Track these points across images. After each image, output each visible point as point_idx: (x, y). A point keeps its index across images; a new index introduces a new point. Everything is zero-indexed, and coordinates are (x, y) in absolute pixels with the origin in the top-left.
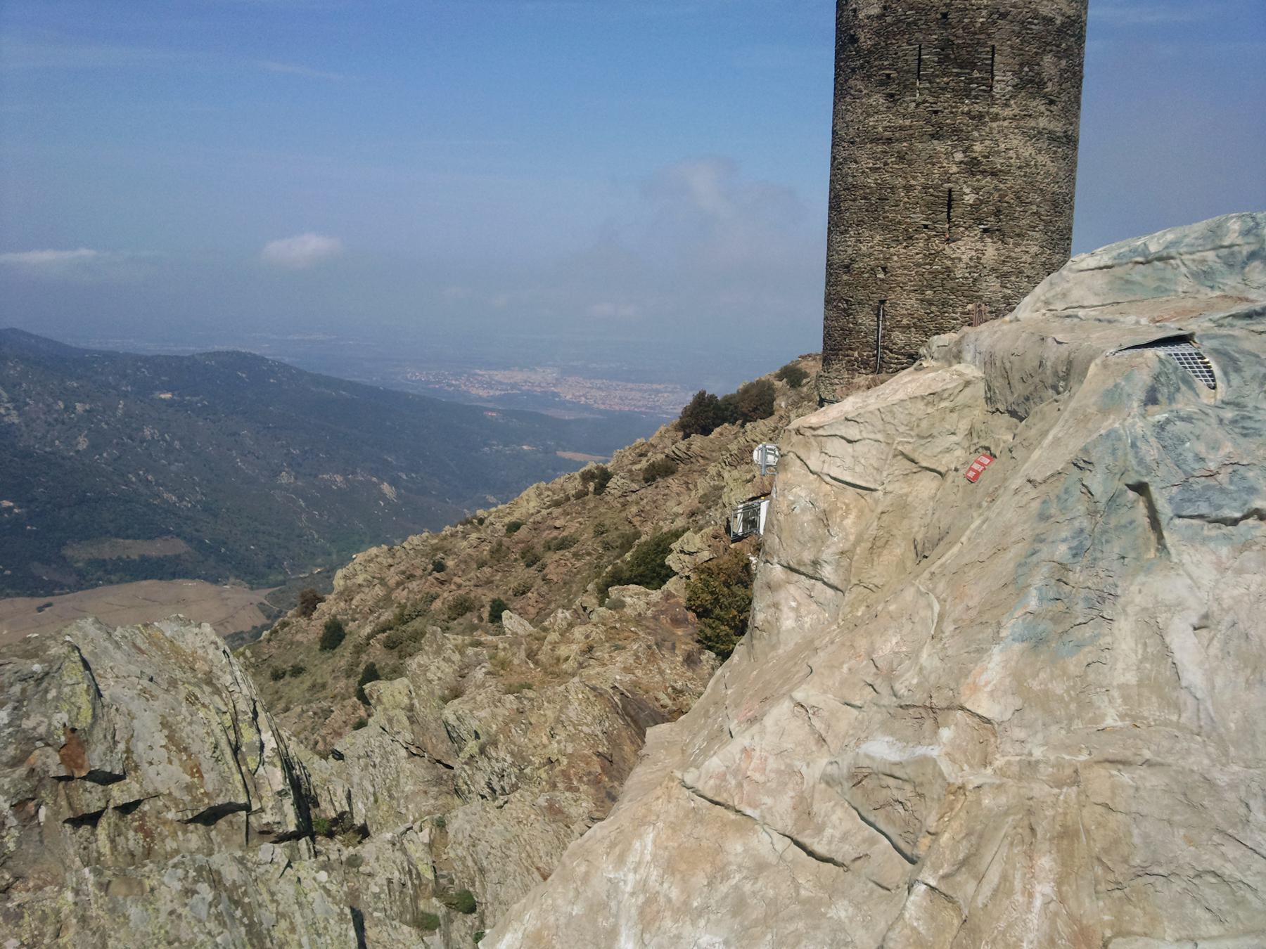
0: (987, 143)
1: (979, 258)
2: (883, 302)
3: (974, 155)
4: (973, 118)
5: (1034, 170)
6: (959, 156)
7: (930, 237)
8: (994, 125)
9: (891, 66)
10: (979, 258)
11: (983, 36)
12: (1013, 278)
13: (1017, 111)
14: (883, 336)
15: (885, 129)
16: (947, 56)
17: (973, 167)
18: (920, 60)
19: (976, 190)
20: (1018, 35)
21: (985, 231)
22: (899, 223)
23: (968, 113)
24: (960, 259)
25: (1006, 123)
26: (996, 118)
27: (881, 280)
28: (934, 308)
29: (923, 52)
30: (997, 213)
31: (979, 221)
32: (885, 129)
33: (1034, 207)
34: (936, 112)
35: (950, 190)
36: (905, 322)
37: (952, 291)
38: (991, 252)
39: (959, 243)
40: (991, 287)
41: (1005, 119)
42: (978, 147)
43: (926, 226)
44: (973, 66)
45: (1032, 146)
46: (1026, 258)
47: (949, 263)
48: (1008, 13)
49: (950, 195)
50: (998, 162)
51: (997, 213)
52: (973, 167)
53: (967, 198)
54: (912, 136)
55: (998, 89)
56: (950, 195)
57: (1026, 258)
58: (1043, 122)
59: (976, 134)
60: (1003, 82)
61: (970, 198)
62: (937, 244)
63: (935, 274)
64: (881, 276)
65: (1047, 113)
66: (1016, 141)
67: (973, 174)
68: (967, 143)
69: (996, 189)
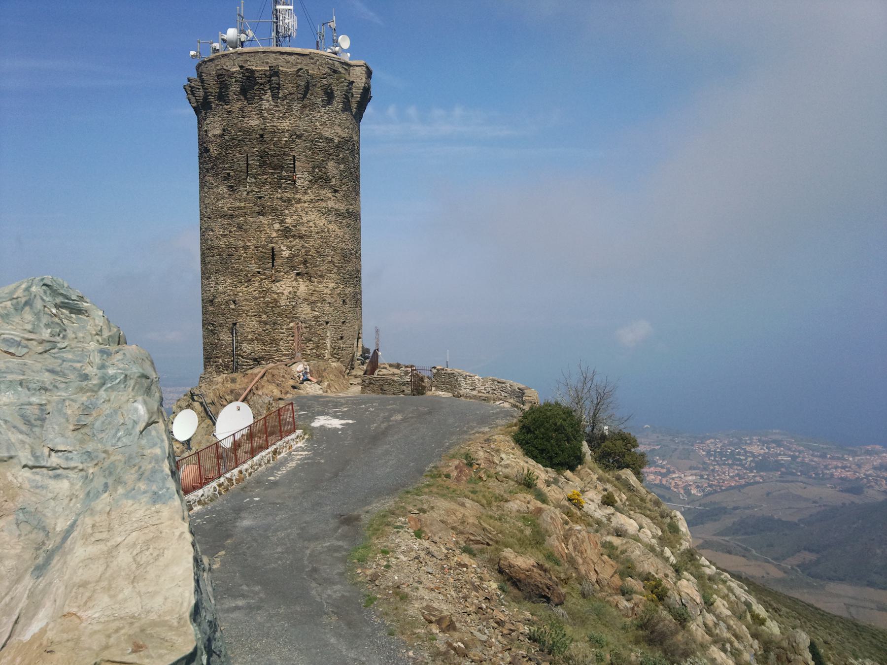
0: (295, 217)
2: (235, 324)
4: (285, 201)
5: (327, 234)
6: (277, 226)
7: (262, 279)
8: (298, 206)
11: (287, 150)
13: (312, 197)
14: (237, 348)
15: (229, 208)
16: (265, 162)
17: (286, 233)
20: (310, 149)
21: (298, 274)
23: (281, 198)
24: (283, 294)
25: (306, 205)
26: (299, 201)
28: (268, 327)
30: (305, 262)
31: (293, 268)
33: (330, 258)
34: (260, 198)
35: (273, 249)
36: (250, 337)
37: (279, 315)
38: (303, 287)
41: (305, 202)
43: (259, 272)
46: (326, 291)
47: (276, 296)
50: (303, 230)
51: (305, 262)
52: (286, 233)
53: (284, 253)
58: (331, 204)
59: (287, 212)
60: (302, 178)
61: (286, 253)
63: (267, 304)
64: (233, 306)
66: (314, 216)
69: (303, 247)
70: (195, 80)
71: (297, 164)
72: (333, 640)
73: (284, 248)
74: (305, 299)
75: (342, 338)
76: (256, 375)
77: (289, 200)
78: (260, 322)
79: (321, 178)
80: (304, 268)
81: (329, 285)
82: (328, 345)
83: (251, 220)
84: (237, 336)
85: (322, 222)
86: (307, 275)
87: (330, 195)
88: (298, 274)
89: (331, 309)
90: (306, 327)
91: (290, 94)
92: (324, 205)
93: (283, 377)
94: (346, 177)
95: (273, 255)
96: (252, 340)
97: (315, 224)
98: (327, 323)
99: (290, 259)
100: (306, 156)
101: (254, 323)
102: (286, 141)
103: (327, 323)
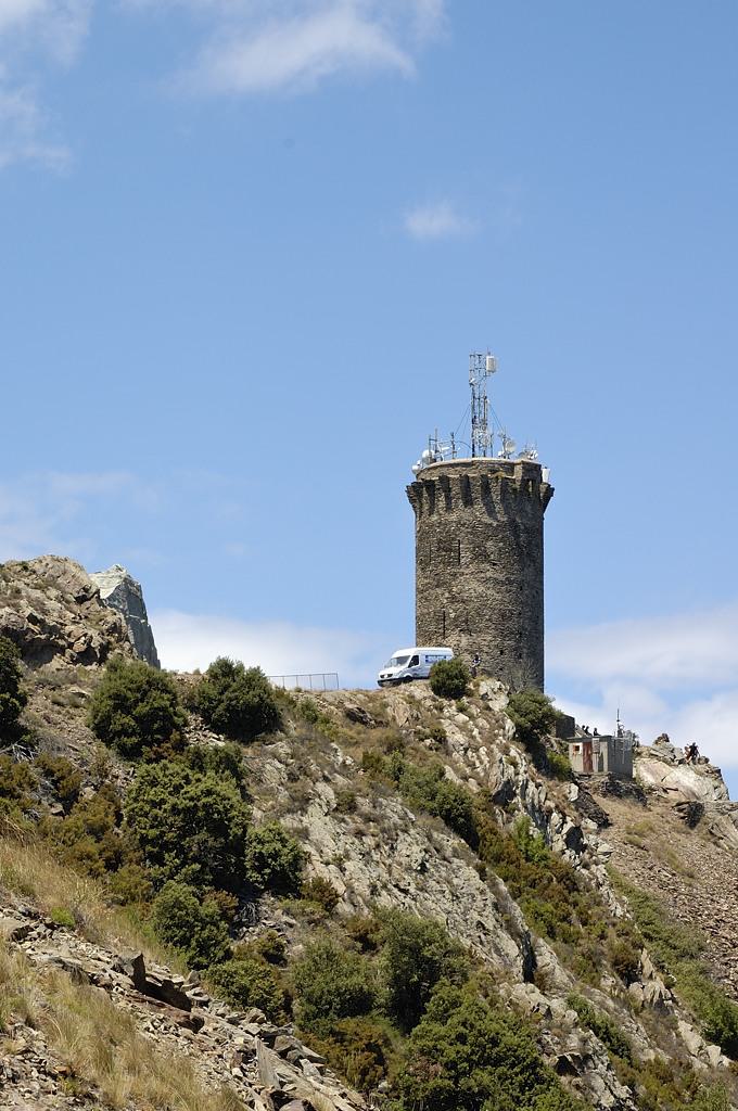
6: (447, 595)
17: (453, 599)
19: (455, 611)
20: (471, 533)
30: (466, 621)
44: (451, 550)
52: (453, 599)
58: (489, 574)
60: (466, 557)
61: (452, 615)
66: (474, 585)
85: (481, 589)
86: (469, 632)
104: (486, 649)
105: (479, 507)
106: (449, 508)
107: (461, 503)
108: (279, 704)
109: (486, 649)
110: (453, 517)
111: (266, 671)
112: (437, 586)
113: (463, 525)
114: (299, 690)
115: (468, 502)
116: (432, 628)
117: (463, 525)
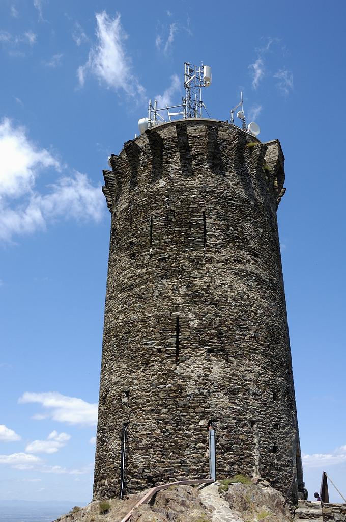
0: (205, 279)
1: (206, 376)
2: (126, 425)
3: (196, 288)
4: (193, 261)
5: (247, 302)
6: (183, 290)
7: (163, 359)
8: (210, 266)
9: (133, 236)
10: (206, 376)
11: (196, 206)
12: (240, 395)
13: (227, 257)
14: (126, 460)
15: (129, 279)
16: (171, 221)
17: (195, 298)
18: (152, 226)
19: (199, 317)
20: (223, 206)
21: (210, 351)
22: (138, 350)
23: (188, 258)
24: (190, 377)
25: (220, 265)
26: (211, 260)
27: (125, 403)
28: (168, 427)
29: (154, 220)
30: (219, 335)
31: (204, 343)
32: (129, 279)
33: (252, 332)
34: (164, 259)
35: (178, 318)
36: (144, 442)
37: (185, 408)
38: (217, 370)
39: (188, 362)
40: (115, 256)
41: (218, 262)
42: (198, 282)
43: (159, 351)
44: (191, 225)
45: (244, 283)
46: (249, 376)
47: (180, 382)
48: (213, 192)
49: (178, 321)
50: (217, 293)
51: (219, 335)
52: (195, 298)
53: (192, 323)
54: (147, 280)
55: (210, 241)
56: (178, 321)
57: (249, 376)
58: (250, 267)
59: (195, 272)
60: (215, 238)
61: (195, 324)
62: (169, 365)
63: (168, 392)
64: (125, 400)
65: (252, 262)
66: (230, 279)
67: (196, 304)
68: (190, 280)
69: (217, 315)
70: (109, 172)
71: (208, 220)
72: (188, 24)
73: (192, 317)
74: (222, 387)
75: (275, 449)
76: (140, 499)
77: (197, 260)
78: (158, 420)
79: (236, 238)
80: (218, 343)
81: (252, 369)
82: (257, 458)
83: (153, 285)
84: (127, 444)
85: (240, 287)
86: (225, 355)
87: (248, 258)
88: (210, 351)
89: (257, 404)
90: (223, 428)
91: (200, 154)
92: (242, 267)
93: (183, 503)
94: (266, 243)
95: (178, 326)
96: (147, 448)
97: (231, 287)
98: (253, 423)
99: (200, 330)
100: (218, 213)
101: (151, 421)
102: (194, 198)
103: (253, 423)
104: (253, 387)
105: (231, 178)
106: (187, 170)
107: (205, 167)
108: (90, 186)
109: (253, 387)
110: (195, 182)
111: (305, 485)
112: (165, 277)
113: (211, 194)
114: (108, 67)
115: (217, 167)
116: (153, 344)
117: (211, 194)
